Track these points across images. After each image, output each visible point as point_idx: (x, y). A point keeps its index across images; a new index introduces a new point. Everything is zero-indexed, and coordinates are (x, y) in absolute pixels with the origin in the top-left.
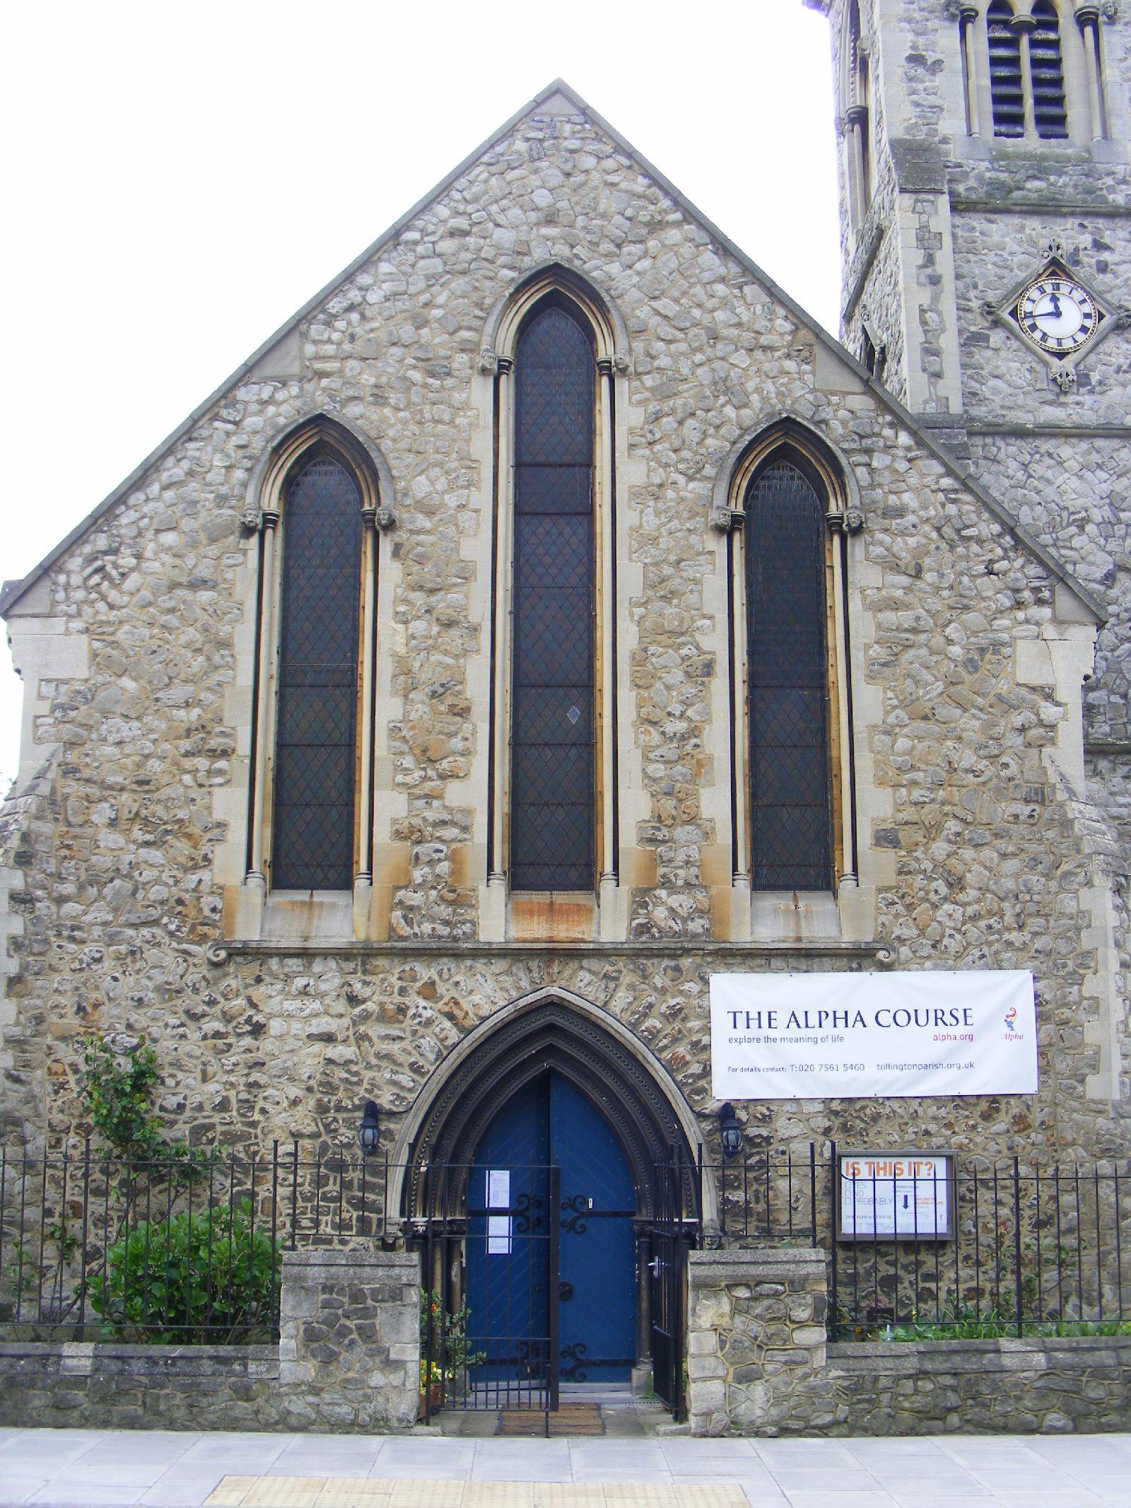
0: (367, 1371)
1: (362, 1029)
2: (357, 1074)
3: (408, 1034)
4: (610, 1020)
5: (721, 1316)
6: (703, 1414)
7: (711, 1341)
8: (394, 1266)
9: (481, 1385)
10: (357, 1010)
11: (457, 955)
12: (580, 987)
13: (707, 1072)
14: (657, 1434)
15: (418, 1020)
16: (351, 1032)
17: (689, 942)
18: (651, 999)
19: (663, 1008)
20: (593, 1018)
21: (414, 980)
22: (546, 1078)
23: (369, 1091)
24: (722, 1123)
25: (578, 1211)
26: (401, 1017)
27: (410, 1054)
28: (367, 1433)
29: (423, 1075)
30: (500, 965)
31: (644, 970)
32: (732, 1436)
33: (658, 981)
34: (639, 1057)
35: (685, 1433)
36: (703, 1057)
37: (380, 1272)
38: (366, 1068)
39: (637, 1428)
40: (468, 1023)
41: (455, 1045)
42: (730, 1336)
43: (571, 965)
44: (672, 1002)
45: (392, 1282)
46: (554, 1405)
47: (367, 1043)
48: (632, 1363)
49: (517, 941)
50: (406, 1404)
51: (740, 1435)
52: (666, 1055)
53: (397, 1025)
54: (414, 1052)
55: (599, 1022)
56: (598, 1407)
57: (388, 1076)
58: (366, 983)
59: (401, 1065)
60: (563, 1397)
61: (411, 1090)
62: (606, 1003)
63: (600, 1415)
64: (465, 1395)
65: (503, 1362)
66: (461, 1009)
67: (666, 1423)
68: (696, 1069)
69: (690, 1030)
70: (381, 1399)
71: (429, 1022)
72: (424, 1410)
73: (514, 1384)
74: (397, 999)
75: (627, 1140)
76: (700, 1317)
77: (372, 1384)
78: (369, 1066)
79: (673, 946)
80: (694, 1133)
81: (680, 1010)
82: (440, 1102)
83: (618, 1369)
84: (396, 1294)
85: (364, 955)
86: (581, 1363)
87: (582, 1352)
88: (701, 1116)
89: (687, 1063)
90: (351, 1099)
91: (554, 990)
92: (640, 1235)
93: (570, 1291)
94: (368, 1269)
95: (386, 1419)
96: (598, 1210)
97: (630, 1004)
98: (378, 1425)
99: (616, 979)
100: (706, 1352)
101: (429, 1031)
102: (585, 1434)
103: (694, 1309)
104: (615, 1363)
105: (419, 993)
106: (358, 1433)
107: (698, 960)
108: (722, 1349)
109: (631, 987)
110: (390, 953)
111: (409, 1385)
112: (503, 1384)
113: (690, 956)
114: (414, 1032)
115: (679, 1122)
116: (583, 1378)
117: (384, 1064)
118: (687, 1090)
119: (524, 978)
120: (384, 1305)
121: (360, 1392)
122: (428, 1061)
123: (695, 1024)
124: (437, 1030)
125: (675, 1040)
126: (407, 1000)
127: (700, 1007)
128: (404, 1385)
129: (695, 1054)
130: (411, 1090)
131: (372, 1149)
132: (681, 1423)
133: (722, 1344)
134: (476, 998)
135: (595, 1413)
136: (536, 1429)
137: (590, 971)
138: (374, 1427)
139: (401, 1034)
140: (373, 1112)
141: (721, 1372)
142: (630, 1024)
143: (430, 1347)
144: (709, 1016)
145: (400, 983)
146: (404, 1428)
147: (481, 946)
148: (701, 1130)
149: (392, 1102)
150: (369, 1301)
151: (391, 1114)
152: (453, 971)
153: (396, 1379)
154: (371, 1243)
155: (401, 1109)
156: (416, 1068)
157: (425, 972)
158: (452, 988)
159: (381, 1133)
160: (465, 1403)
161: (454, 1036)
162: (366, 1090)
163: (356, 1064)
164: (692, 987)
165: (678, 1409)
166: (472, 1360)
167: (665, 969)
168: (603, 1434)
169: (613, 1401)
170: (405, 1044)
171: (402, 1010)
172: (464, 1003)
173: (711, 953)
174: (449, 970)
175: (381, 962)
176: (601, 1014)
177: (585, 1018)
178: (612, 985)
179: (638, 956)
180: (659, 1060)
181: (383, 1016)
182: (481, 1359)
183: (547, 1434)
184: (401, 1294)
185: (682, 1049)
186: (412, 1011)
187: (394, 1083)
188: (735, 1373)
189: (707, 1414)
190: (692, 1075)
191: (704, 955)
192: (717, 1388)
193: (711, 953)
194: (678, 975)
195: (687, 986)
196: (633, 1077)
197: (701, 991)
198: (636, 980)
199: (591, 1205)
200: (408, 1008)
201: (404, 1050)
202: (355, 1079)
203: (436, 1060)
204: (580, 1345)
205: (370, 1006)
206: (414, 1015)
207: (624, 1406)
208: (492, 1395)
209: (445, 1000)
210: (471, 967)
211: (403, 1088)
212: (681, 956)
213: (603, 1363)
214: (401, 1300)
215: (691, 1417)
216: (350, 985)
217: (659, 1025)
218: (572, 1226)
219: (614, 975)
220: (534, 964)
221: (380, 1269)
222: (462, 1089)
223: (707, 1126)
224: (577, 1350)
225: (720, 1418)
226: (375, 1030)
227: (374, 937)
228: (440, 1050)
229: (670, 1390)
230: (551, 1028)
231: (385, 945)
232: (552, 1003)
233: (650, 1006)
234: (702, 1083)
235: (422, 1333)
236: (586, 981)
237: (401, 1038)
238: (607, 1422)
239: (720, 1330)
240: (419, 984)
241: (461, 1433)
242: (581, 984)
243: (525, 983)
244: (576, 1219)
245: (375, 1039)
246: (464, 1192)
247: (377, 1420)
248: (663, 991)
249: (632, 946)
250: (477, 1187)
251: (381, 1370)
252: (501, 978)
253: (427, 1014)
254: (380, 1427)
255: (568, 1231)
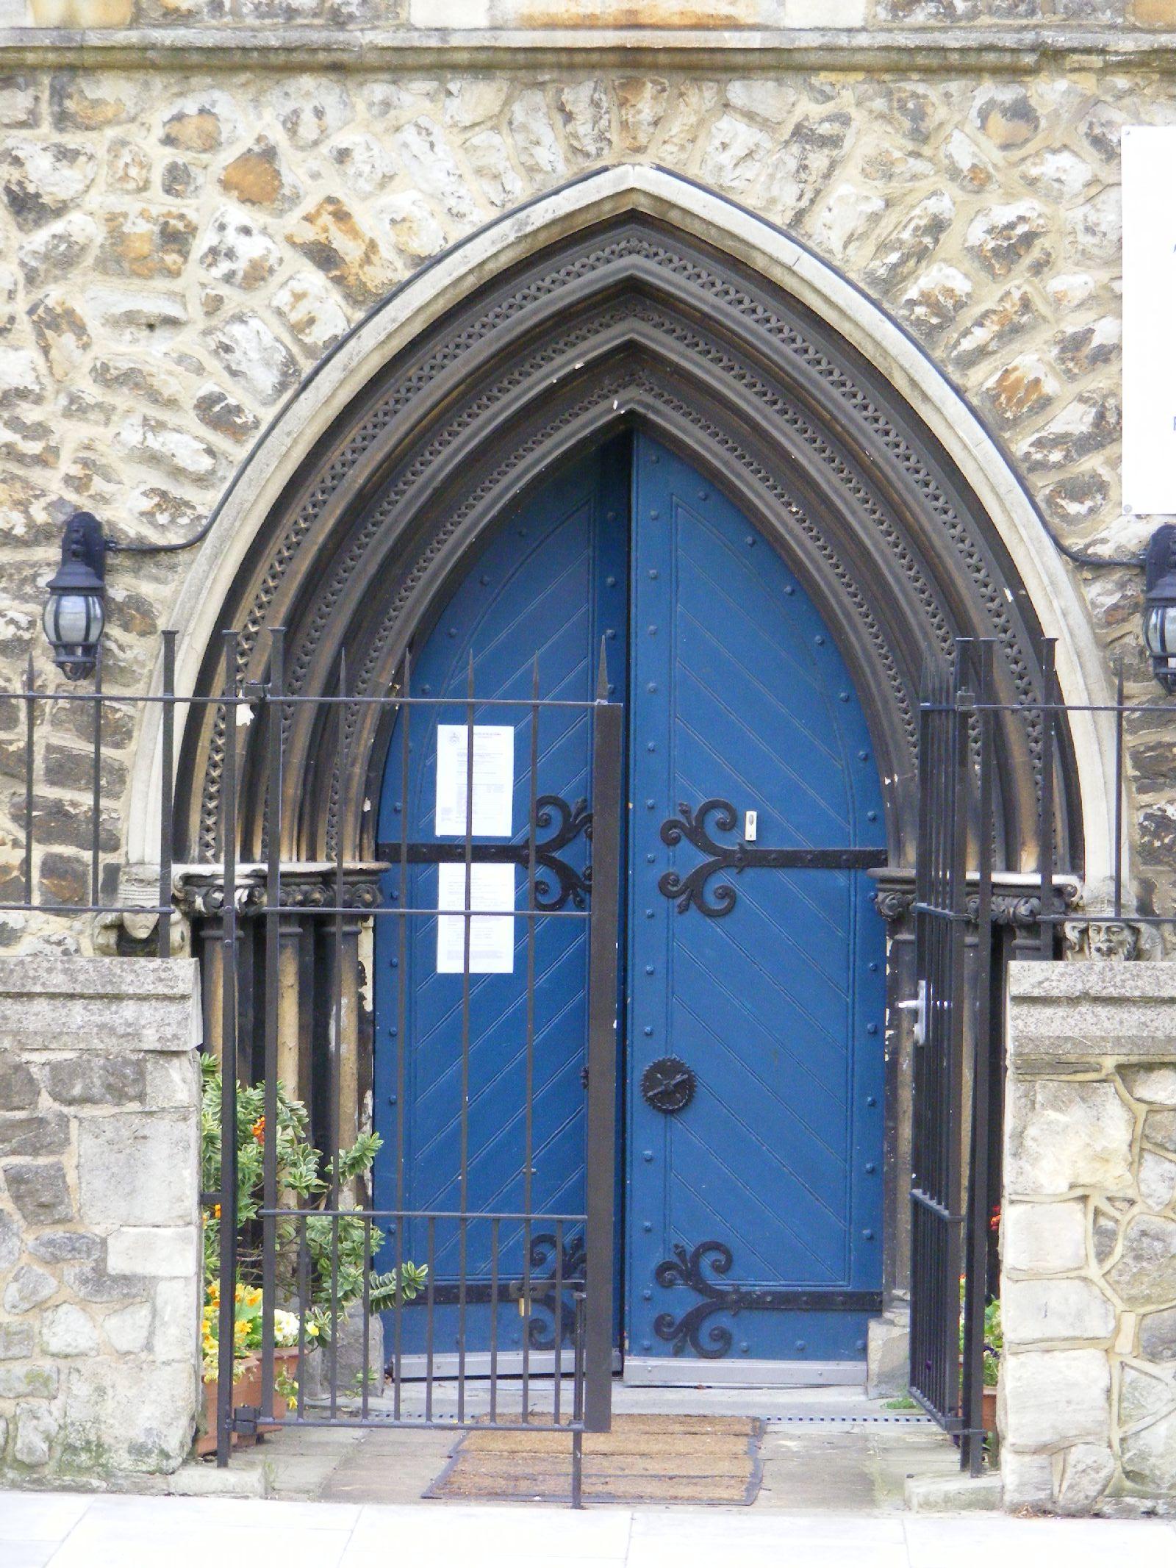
0: (40, 1306)
1: (55, 294)
2: (40, 431)
3: (195, 311)
4: (809, 268)
5: (1103, 1158)
6: (1038, 1450)
7: (1069, 1233)
8: (118, 998)
9: (413, 1364)
10: (40, 238)
11: (341, 68)
12: (718, 168)
13: (1105, 431)
14: (907, 1505)
15: (224, 266)
16: (20, 306)
17: (1061, 28)
18: (941, 206)
19: (977, 234)
20: (760, 263)
21: (211, 144)
22: (622, 440)
23: (79, 484)
24: (1151, 586)
25: (709, 848)
26: (171, 259)
27: (200, 370)
28: (40, 1485)
29: (238, 433)
30: (477, 98)
31: (918, 116)
32: (1128, 1513)
33: (963, 148)
34: (900, 383)
35: (987, 1503)
36: (1097, 382)
37: (78, 1014)
38: (67, 414)
39: (855, 1484)
40: (376, 277)
41: (338, 344)
42: (1127, 1222)
43: (693, 97)
44: (1004, 215)
45: (112, 1044)
46: (596, 1415)
47: (68, 339)
48: (872, 1305)
49: (530, 24)
50: (160, 1401)
51: (1151, 1513)
52: (982, 377)
53: (161, 284)
54: (213, 365)
55: (777, 274)
56: (758, 1428)
57: (133, 435)
58: (66, 155)
59: (171, 403)
60: (621, 1398)
61: (202, 480)
62: (799, 216)
63: (752, 1452)
64: (366, 1389)
65: (478, 1295)
66: (355, 233)
67: (941, 1472)
68: (1072, 419)
69: (1058, 300)
70: (82, 1389)
71: (257, 275)
72: (211, 1427)
73: (510, 1360)
74: (160, 203)
75: (864, 638)
76: (1035, 1160)
77: (55, 1345)
78: (76, 408)
79: (1009, 40)
80: (1062, 605)
81: (1029, 239)
82: (293, 516)
83: (822, 1318)
84: (126, 1082)
85: (59, 68)
86: (718, 1302)
87: (722, 1269)
88: (1087, 565)
89: (1046, 402)
90: (23, 505)
91: (641, 177)
92: (897, 922)
93: (688, 1087)
94: (41, 1005)
95: (97, 1448)
96: (773, 845)
97: (875, 218)
98: (78, 1464)
99: (833, 142)
100: (1054, 1263)
101: (256, 300)
102: (692, 1500)
103: (1019, 1135)
104: (820, 1302)
105: (226, 185)
106: (14, 1485)
107: (1088, 84)
108: (1102, 1255)
109: (882, 168)
110: (139, 62)
111: (163, 1350)
112: (478, 1362)
113: (1062, 72)
114: (214, 305)
115: (1015, 581)
116: (723, 1347)
117: (121, 399)
118: (1043, 484)
119: (547, 136)
120: (87, 1111)
121: (19, 1369)
122: (254, 392)
123: (1072, 281)
124: (283, 298)
125: (1012, 331)
126: (189, 207)
127: (1090, 230)
128: (149, 1347)
129: (1071, 377)
130: (202, 480)
131: (85, 658)
132: (978, 1471)
133: (1104, 1240)
134: (401, 200)
135: (741, 1445)
136: (549, 1486)
137: (750, 116)
138: (63, 1468)
139: (173, 310)
140: (88, 547)
141: (1098, 1326)
142: (874, 280)
143: (242, 1242)
144: (1115, 260)
145: (169, 155)
146: (151, 1474)
147: (416, 40)
148: (1088, 608)
149: (148, 515)
150: (46, 1103)
151: (145, 553)
152: (331, 117)
153: (125, 1328)
154: (84, 932)
155: (174, 538)
156: (217, 414)
157: (244, 116)
158: (329, 169)
159: (110, 610)
160: (365, 1411)
161: (333, 314)
162: (68, 480)
163: (39, 400)
164: (1071, 168)
165: (974, 1440)
166: (387, 1283)
167: (984, 115)
168: (749, 1492)
169: (807, 1415)
170: (186, 340)
171: (174, 238)
172: (367, 218)
173: (1126, 65)
174: (319, 113)
175: (111, 90)
176: (784, 250)
177: (733, 263)
178: (819, 160)
179: (901, 71)
180: (958, 391)
181: (118, 258)
182: (412, 1282)
183: (577, 1499)
184: (141, 1075)
185: (1031, 359)
186: (200, 245)
187: (153, 459)
188: (1140, 1327)
189: (1053, 1450)
190: (1058, 441)
191: (1106, 70)
192: (1087, 1372)
193: (1126, 65)
194: (1022, 128)
195: (1052, 166)
196: (879, 446)
197: (1095, 181)
198: (893, 142)
199: (751, 832)
200: (192, 230)
201: (181, 359)
202: (33, 448)
203: (282, 387)
204: (715, 1246)
205: (78, 225)
206: (213, 251)
207: (838, 1427)
208: (445, 1392)
209: (308, 205)
210: (387, 105)
211: (178, 473)
212: (1033, 71)
213: (783, 1302)
214: (141, 1097)
215: (1006, 1455)
216: (17, 161)
217: (961, 286)
218: (689, 893)
219: (825, 129)
220: (579, 96)
221: (78, 1006)
222: (358, 477)
223: (1103, 593)
224: (706, 1262)
225: (1093, 1464)
226: (94, 297)
227: (89, 14)
228: (291, 361)
229: (953, 1384)
230: (631, 294)
231: (121, 37)
232: (634, 217)
233: (937, 227)
234: (1093, 463)
235: (205, 1201)
236: (738, 150)
237: (172, 322)
238: (769, 1468)
239: (1097, 1201)
240: (228, 156)
241: (327, 1492)
242: (726, 159)
243: (552, 156)
244: (703, 874)
245: (94, 327)
246: (367, 794)
247: (70, 1448)
248: (978, 180)
249: (882, 39)
250: (400, 770)
251: (84, 1304)
252: (480, 137)
253: (249, 249)
254: (80, 1470)
255: (683, 909)
